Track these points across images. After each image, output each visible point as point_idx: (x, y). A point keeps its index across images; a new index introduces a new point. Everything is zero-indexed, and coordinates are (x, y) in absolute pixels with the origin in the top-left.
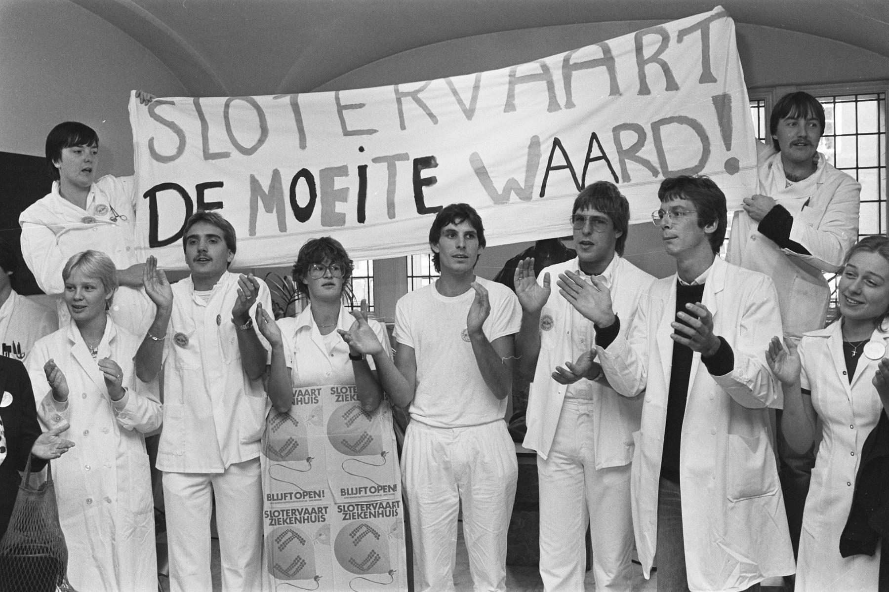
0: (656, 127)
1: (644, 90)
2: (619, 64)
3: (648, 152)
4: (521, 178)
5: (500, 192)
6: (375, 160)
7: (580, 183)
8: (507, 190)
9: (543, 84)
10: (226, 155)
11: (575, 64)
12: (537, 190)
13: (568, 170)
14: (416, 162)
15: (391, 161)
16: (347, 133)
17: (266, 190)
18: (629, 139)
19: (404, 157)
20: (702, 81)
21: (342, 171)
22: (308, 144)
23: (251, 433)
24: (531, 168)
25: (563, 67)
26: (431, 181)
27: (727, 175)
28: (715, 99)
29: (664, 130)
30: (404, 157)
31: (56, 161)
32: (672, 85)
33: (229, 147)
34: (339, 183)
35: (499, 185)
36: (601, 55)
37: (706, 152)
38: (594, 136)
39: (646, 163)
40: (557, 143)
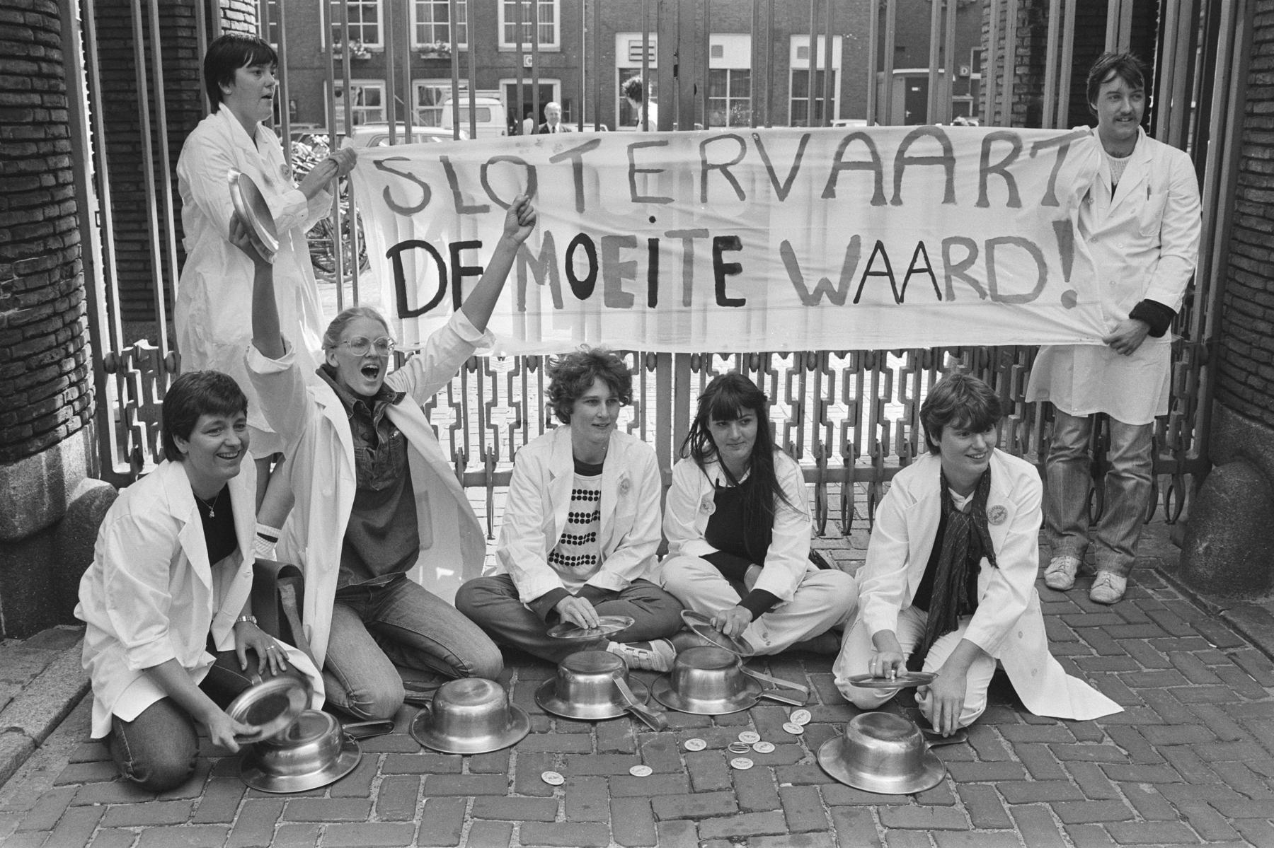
0: (990, 244)
1: (983, 202)
2: (959, 167)
3: (978, 271)
4: (835, 280)
5: (811, 293)
6: (670, 234)
7: (900, 294)
8: (819, 292)
9: (872, 173)
10: (485, 209)
11: (911, 158)
12: (852, 293)
13: (887, 278)
14: (717, 240)
15: (688, 237)
16: (636, 199)
17: (536, 256)
18: (959, 254)
19: (705, 233)
20: (1044, 203)
21: (630, 242)
22: (586, 207)
23: (156, 802)
24: (848, 270)
25: (896, 159)
26: (735, 269)
27: (1063, 309)
28: (1056, 224)
29: (998, 252)
30: (705, 233)
31: (226, 84)
32: (1014, 202)
33: (488, 201)
34: (625, 255)
35: (811, 286)
36: (941, 154)
37: (1042, 281)
38: (921, 245)
39: (975, 283)
40: (879, 246)
